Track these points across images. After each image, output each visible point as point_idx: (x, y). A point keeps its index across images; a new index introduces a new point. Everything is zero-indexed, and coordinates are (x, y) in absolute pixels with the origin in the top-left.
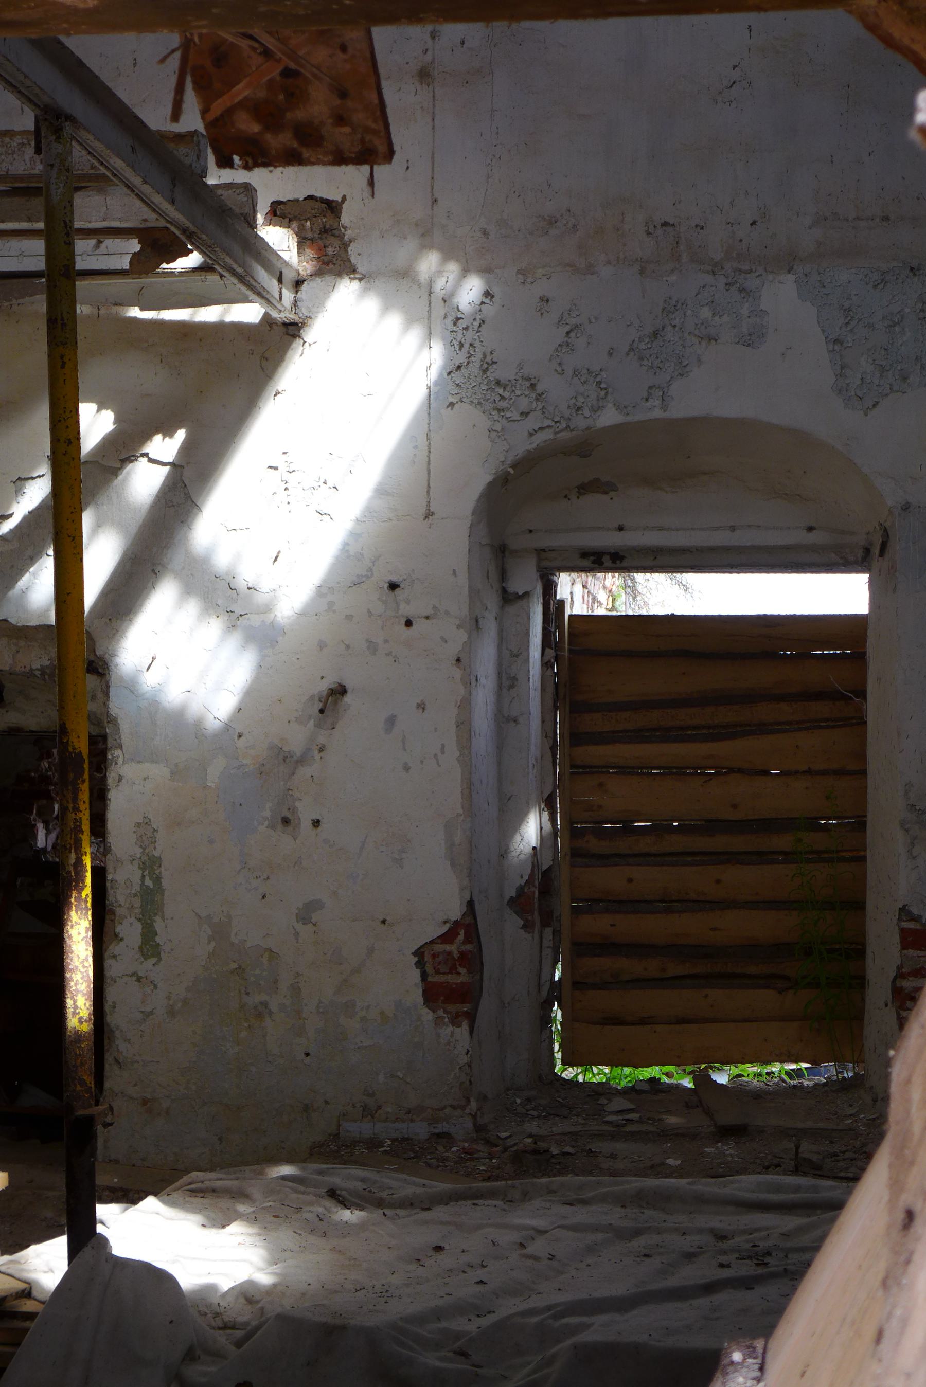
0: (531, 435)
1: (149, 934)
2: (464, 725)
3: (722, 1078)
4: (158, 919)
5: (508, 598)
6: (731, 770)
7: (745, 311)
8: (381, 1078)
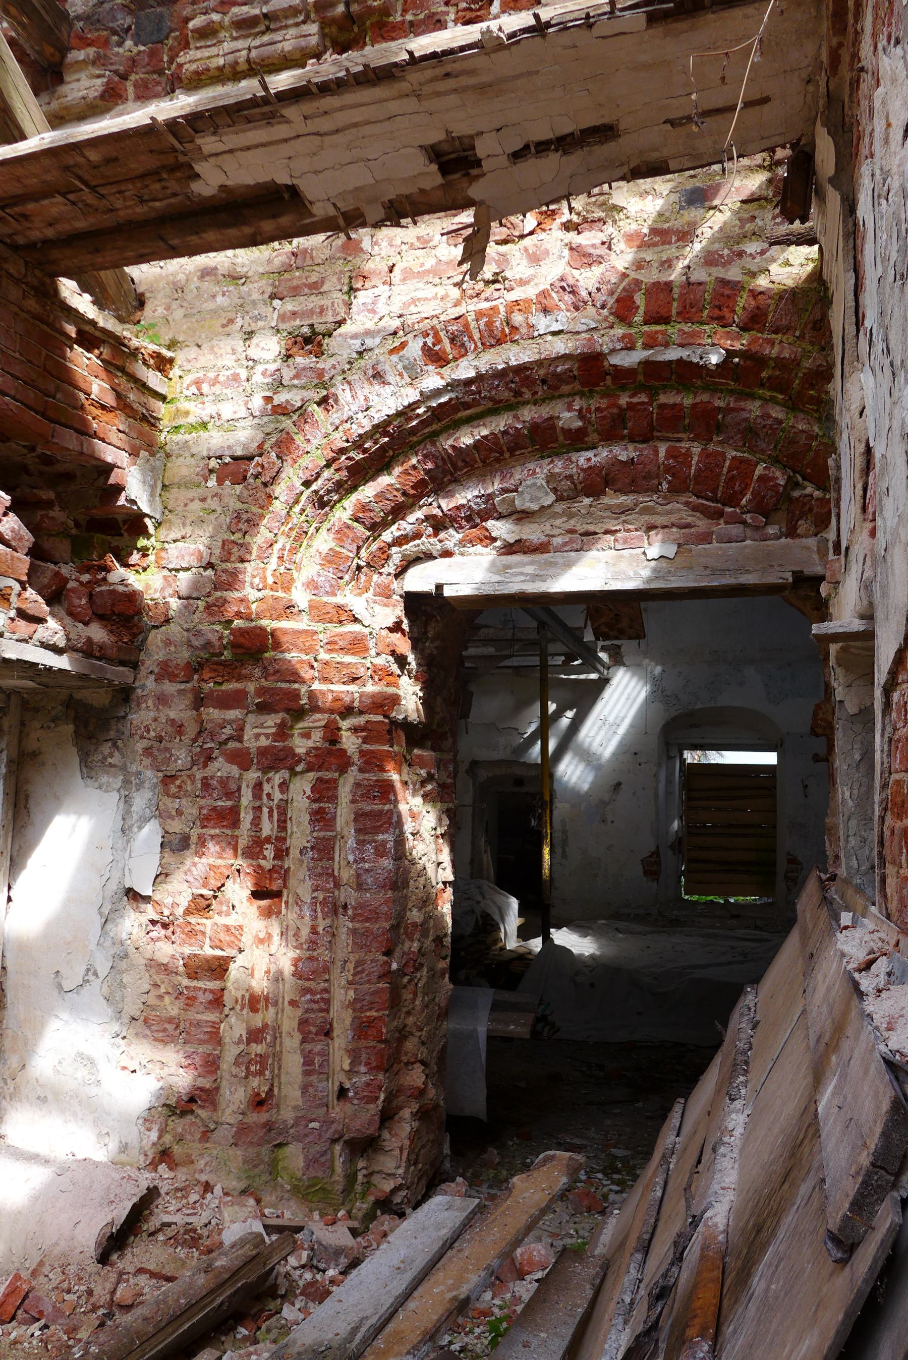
1: (564, 852)
2: (656, 795)
3: (732, 901)
5: (670, 758)
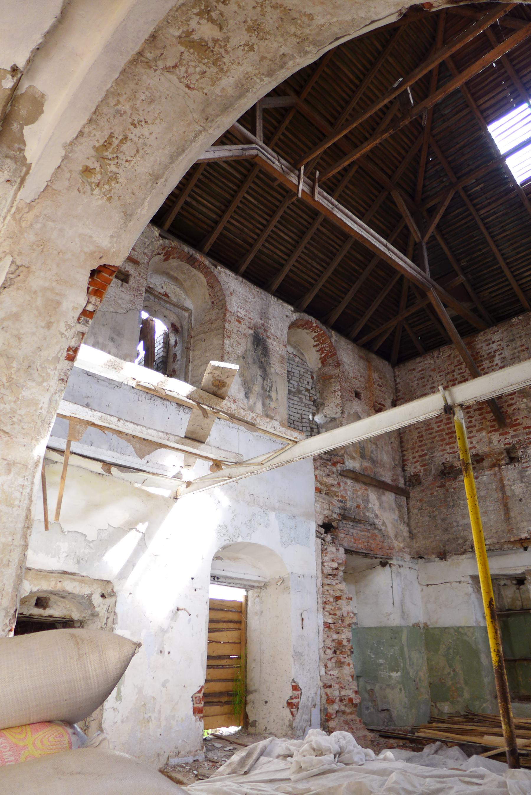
0: (225, 540)
4: (122, 686)
6: (213, 641)
7: (266, 519)
8: (180, 741)
